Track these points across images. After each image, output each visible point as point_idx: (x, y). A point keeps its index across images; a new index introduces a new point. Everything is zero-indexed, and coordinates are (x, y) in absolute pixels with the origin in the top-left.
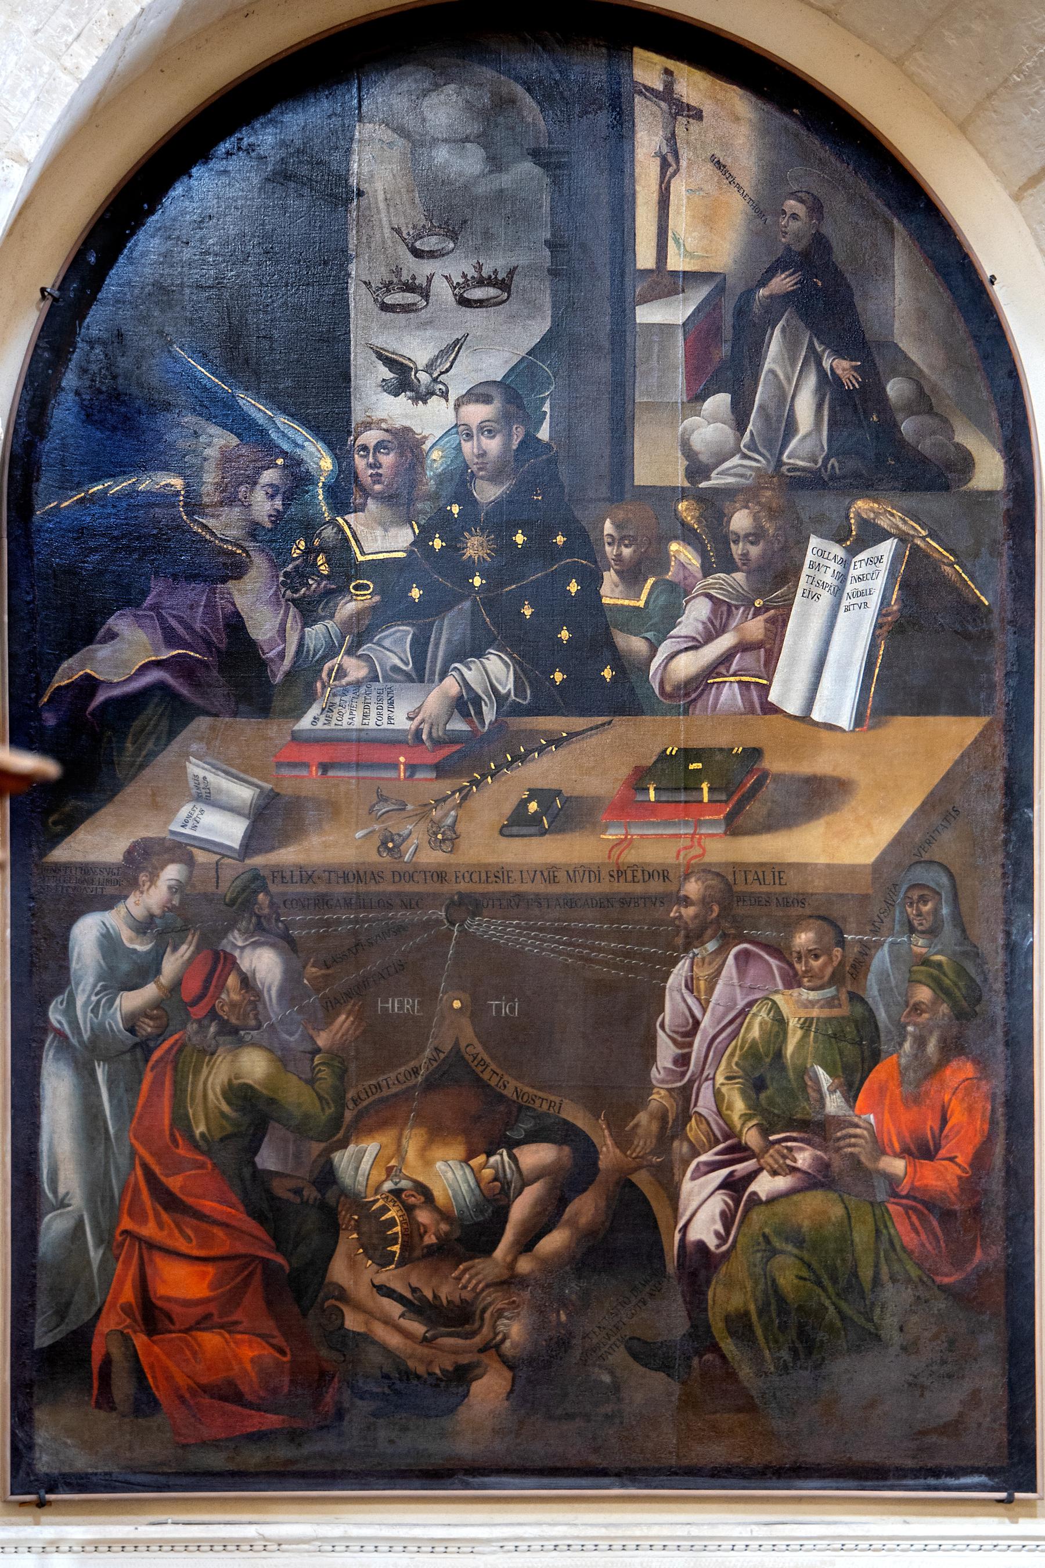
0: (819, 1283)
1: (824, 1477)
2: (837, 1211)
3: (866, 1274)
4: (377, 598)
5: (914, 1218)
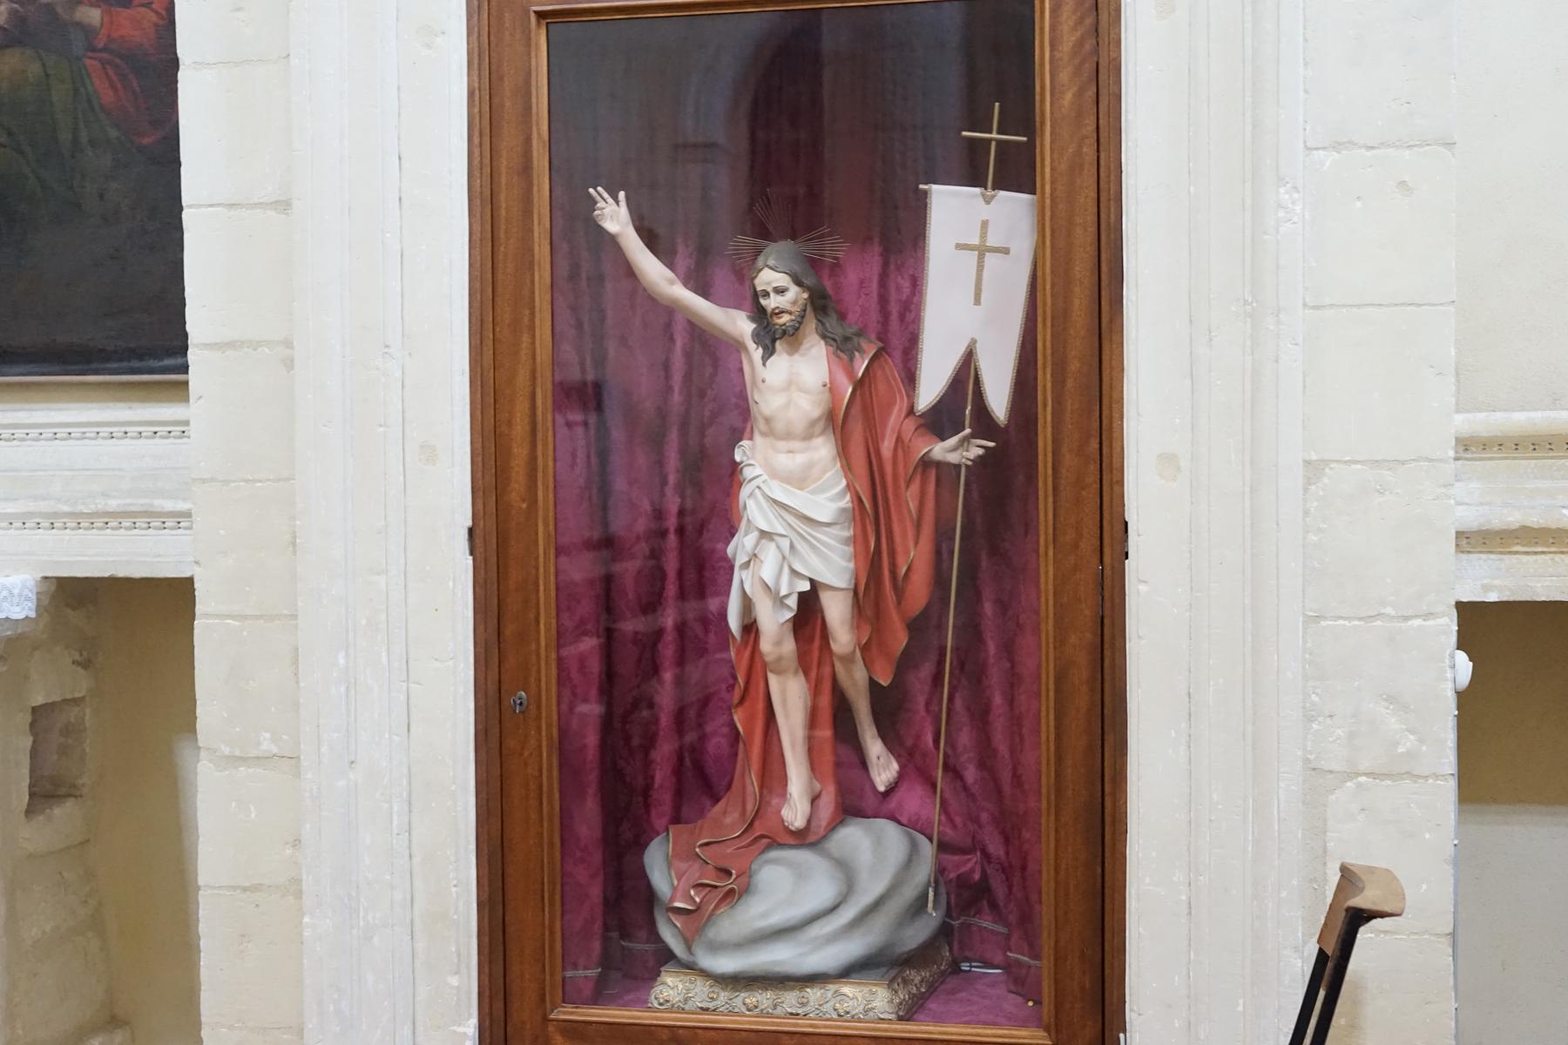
0: (21, 153)
1: (30, 362)
2: (35, 69)
3: (65, 136)
4: (622, 195)
5: (111, 72)
